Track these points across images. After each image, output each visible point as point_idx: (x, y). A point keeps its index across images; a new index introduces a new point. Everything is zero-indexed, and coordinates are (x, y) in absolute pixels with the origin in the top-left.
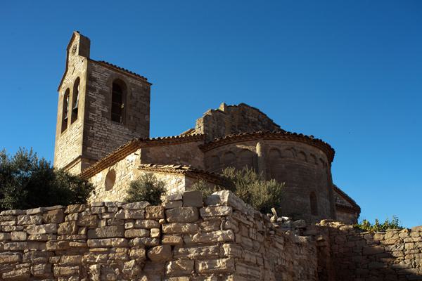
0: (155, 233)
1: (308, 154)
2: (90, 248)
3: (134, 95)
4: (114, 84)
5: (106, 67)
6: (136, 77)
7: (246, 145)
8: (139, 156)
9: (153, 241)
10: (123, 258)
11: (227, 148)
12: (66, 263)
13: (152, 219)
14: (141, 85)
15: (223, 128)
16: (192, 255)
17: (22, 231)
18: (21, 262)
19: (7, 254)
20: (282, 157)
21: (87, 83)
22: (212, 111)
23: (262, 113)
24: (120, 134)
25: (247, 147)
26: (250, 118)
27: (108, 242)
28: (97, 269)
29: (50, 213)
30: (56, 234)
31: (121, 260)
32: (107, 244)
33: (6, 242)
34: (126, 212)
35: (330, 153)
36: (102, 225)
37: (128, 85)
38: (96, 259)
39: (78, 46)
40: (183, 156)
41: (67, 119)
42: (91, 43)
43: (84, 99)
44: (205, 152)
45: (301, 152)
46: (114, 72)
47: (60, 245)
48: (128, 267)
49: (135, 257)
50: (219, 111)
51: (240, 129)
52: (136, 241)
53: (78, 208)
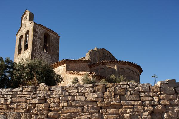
0: (156, 99)
1: (134, 71)
2: (123, 105)
3: (53, 41)
4: (44, 35)
5: (42, 27)
6: (54, 33)
7: (110, 65)
8: (66, 67)
9: (156, 103)
10: (142, 111)
11: (101, 66)
12: (110, 113)
13: (153, 92)
14: (56, 37)
15: (97, 58)
16: (176, 110)
17: (82, 95)
18: (83, 112)
19: (74, 108)
20: (125, 72)
21: (33, 33)
22: (93, 50)
23: (111, 53)
24: (46, 57)
25: (110, 67)
26: (106, 55)
27: (133, 103)
28: (129, 116)
29: (98, 87)
30: (103, 98)
31: (141, 112)
32: (132, 104)
33: (73, 101)
34: (140, 88)
35: (141, 70)
36: (128, 94)
38: (127, 111)
40: (82, 69)
41: (21, 49)
42: (34, 16)
43: (32, 40)
44: (90, 68)
45: (132, 71)
46: (45, 30)
47: (106, 104)
48: (145, 116)
49: (148, 110)
50: (95, 50)
51: (103, 59)
52: (147, 102)
53: (114, 85)
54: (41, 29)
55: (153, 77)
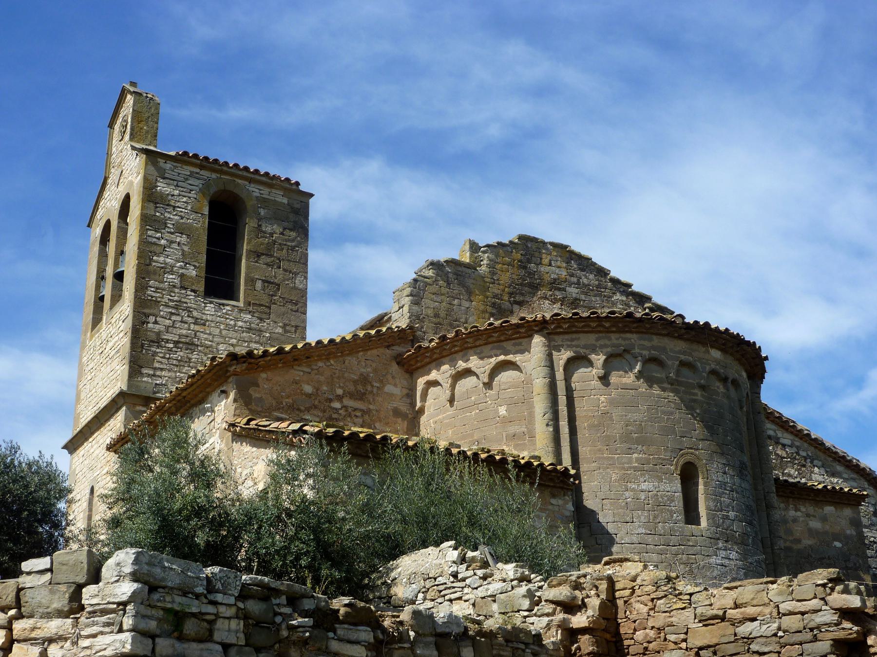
37: (250, 204)
39: (129, 120)
40: (351, 387)
46: (214, 176)
54: (192, 175)
55: (40, 452)
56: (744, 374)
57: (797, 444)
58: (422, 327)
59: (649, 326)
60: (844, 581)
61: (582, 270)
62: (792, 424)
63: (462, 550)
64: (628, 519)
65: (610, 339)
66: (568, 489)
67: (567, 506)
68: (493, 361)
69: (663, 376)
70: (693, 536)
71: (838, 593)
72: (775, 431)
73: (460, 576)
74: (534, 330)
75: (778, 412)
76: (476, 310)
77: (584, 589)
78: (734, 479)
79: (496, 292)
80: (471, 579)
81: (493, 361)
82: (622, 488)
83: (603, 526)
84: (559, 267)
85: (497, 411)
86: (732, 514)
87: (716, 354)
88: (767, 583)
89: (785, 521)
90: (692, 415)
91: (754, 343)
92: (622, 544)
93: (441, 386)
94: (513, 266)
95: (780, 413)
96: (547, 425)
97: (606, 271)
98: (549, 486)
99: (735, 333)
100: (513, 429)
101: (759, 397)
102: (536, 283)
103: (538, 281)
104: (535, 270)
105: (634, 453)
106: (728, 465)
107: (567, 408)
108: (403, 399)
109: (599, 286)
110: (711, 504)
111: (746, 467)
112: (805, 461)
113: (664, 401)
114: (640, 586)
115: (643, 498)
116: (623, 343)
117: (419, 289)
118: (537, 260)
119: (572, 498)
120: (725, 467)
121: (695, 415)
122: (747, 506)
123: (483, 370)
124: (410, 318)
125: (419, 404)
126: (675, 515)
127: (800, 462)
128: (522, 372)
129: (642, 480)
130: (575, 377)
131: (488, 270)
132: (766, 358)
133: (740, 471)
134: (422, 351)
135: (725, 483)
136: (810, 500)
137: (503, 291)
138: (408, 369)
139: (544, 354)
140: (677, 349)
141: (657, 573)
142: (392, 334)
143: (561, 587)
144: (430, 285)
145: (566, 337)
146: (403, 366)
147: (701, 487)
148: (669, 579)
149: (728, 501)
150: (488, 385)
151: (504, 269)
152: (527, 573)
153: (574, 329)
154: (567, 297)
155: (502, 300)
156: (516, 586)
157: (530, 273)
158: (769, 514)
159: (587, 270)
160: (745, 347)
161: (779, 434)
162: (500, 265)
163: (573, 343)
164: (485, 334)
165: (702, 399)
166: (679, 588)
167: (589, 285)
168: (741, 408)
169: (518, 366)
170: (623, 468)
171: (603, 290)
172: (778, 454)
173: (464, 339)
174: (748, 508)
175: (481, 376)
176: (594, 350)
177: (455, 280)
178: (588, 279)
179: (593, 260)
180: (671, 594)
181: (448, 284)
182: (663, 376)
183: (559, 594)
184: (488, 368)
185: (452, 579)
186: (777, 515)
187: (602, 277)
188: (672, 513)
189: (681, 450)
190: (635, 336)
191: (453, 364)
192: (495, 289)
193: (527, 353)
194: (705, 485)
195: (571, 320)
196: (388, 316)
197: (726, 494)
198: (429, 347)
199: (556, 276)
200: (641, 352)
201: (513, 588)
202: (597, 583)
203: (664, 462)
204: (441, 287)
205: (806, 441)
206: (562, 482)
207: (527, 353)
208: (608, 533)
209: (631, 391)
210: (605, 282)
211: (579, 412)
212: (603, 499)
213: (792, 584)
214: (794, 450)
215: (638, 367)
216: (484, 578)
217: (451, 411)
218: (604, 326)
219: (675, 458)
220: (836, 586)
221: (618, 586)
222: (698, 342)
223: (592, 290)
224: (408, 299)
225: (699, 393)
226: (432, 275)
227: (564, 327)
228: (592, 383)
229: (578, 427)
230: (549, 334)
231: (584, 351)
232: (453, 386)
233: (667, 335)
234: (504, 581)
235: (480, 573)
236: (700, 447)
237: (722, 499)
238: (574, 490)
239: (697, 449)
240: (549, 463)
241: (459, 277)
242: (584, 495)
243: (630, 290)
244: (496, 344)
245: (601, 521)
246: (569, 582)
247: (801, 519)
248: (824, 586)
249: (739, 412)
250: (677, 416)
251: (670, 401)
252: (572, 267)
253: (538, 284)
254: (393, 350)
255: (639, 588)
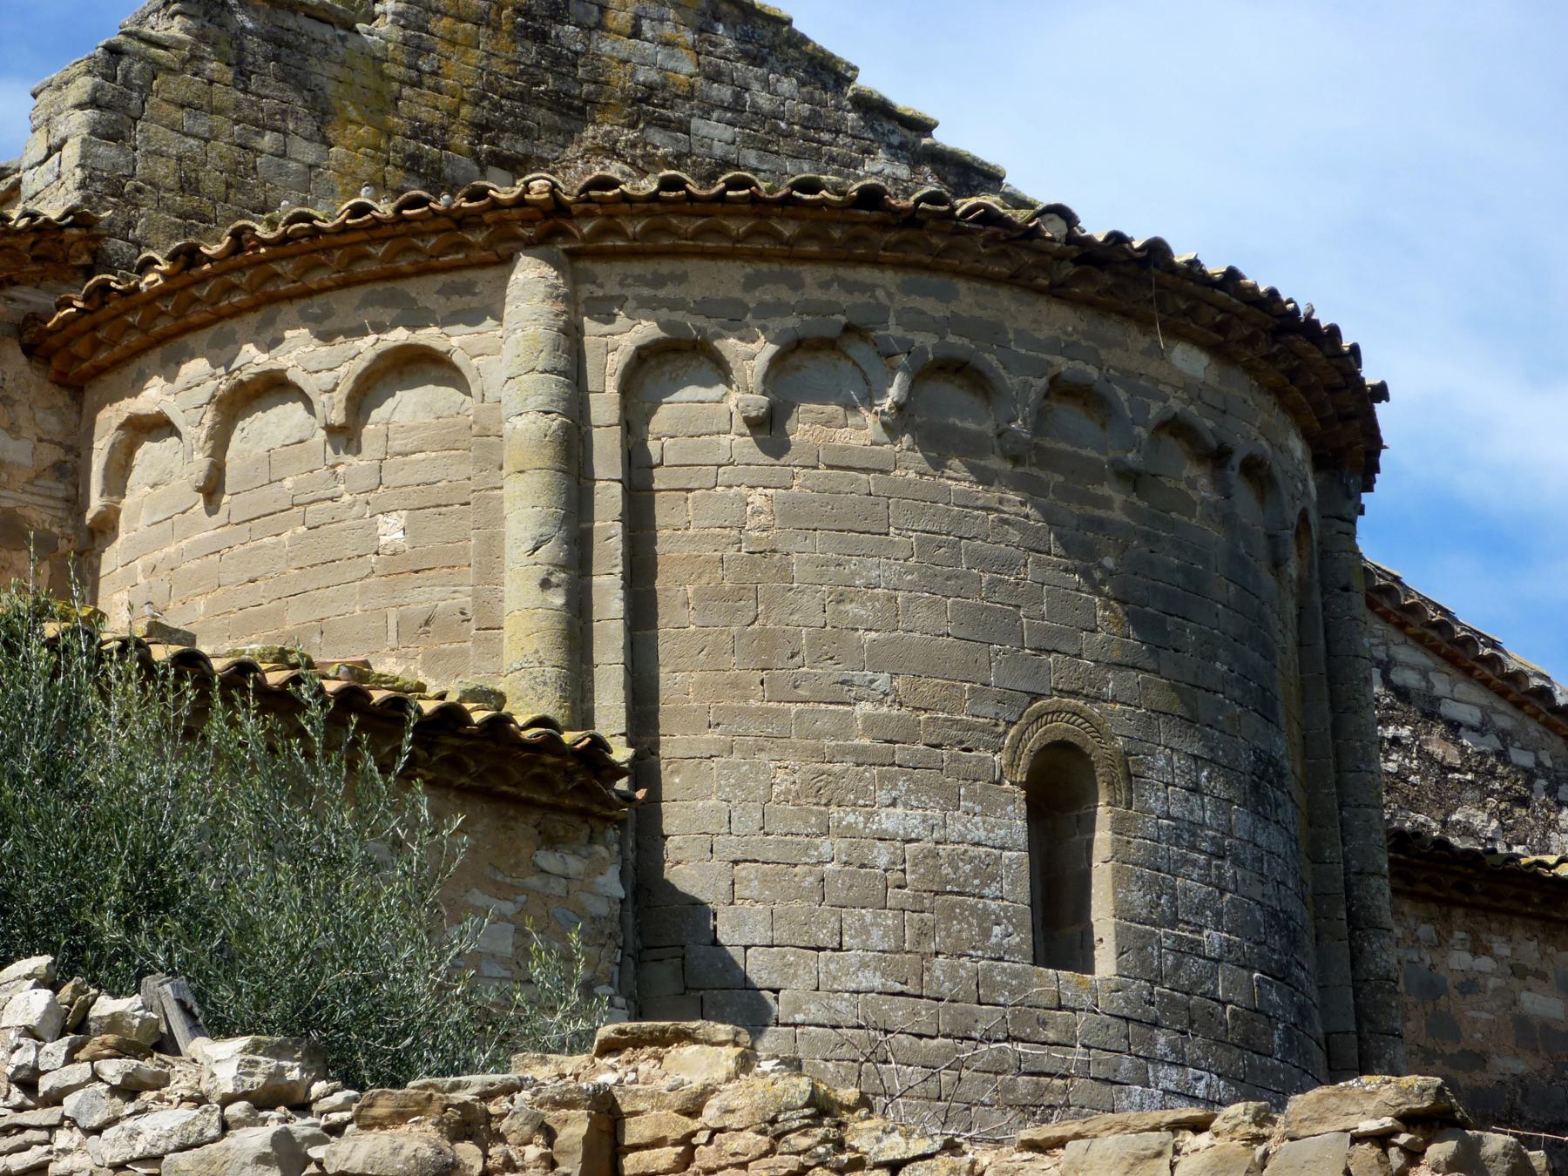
56: (1297, 446)
57: (1503, 722)
58: (130, 225)
59: (942, 245)
60: (1464, 1125)
61: (755, 60)
62: (1487, 651)
63: (77, 990)
64: (823, 937)
65: (796, 284)
66: (607, 819)
67: (600, 879)
68: (368, 347)
69: (988, 428)
70: (1060, 1008)
71: (1436, 1170)
72: (1424, 674)
73: (45, 1084)
74: (517, 238)
75: (1438, 607)
76: (343, 175)
77: (500, 1138)
78: (1227, 812)
79: (423, 116)
80: (79, 1094)
81: (368, 347)
82: (806, 822)
83: (731, 959)
84: (668, 44)
85: (371, 533)
86: (1212, 939)
87: (1190, 361)
88: (1176, 1127)
89: (1432, 988)
90: (1086, 575)
91: (1334, 331)
92: (796, 1025)
93: (178, 434)
94: (497, 29)
95: (1446, 612)
96: (545, 584)
97: (841, 68)
98: (529, 804)
99: (1262, 289)
100: (425, 597)
101: (1351, 535)
102: (578, 97)
103: (585, 88)
104: (579, 47)
105: (858, 699)
106: (1211, 761)
107: (624, 527)
108: (40, 482)
109: (810, 122)
110: (1136, 896)
111: (1281, 775)
112: (1529, 783)
113: (985, 520)
114: (714, 1132)
115: (883, 861)
116: (845, 299)
117: (127, 82)
118: (588, 13)
119: (621, 852)
120: (1199, 770)
121: (1098, 575)
122: (1274, 914)
123: (326, 378)
124: (82, 186)
125: (96, 502)
126: (997, 930)
127: (1508, 789)
128: (465, 388)
129: (883, 796)
130: (663, 418)
131: (397, 34)
132: (1381, 392)
133: (1255, 787)
134: (115, 304)
135: (1196, 827)
136: (1528, 915)
137: (453, 114)
138: (64, 374)
139: (549, 327)
140: (1044, 333)
141: (780, 1085)
142: (9, 240)
143: (405, 1128)
144: (170, 71)
145: (637, 268)
146: (47, 360)
147: (1103, 837)
148: (821, 1108)
149: (1199, 890)
150: (345, 436)
151: (460, 37)
152: (295, 1075)
153: (666, 241)
154: (689, 154)
155: (445, 147)
156: (241, 1123)
157: (557, 59)
158: (1361, 951)
159: (772, 59)
160: (1302, 344)
161: (1441, 685)
162: (446, 22)
163: (662, 293)
164: (340, 247)
165: (1126, 519)
166: (855, 1143)
167: (777, 116)
168: (1277, 564)
169: (456, 369)
170: (817, 753)
171: (826, 136)
172: (1430, 756)
173: (263, 262)
174: (1278, 920)
175: (320, 401)
176: (736, 323)
177: (267, 59)
178: (774, 93)
179: (795, 25)
180: (822, 1164)
181: (241, 73)
182: (988, 428)
183: (387, 1152)
184: (348, 372)
185: (17, 1096)
186: (1388, 955)
187: (825, 88)
188: (986, 921)
189: (1036, 697)
190: (889, 278)
191: (222, 357)
192: (422, 107)
193: (489, 322)
194: (1119, 826)
195: (657, 206)
196: (11, 180)
197: (1194, 863)
198: (136, 289)
199: (654, 76)
200: (910, 336)
201: (225, 1127)
202: (551, 1116)
203: (970, 738)
204: (211, 82)
205: (1535, 716)
206: (582, 789)
207: (489, 322)
208: (746, 985)
209: (864, 476)
210: (838, 108)
211: (667, 545)
212: (736, 862)
213: (1265, 1131)
214: (1491, 743)
215: (894, 392)
216: (128, 1090)
217: (207, 529)
218: (776, 236)
219: (1010, 724)
220: (1428, 1143)
221: (635, 1131)
222: (1127, 315)
223: (788, 135)
224: (81, 118)
225: (1118, 498)
226: (181, 35)
227: (630, 230)
228: (725, 440)
229: (660, 598)
230: (573, 255)
231: (701, 321)
232: (220, 439)
233: (1013, 280)
234: (199, 1100)
235: (113, 1070)
236: (1109, 690)
237: (1179, 882)
238: (631, 826)
239: (1096, 699)
240: (530, 717)
241: (284, 51)
242: (669, 845)
243: (925, 141)
244: (380, 287)
245: (723, 937)
246: (436, 1106)
247: (1492, 983)
248: (1382, 1139)
249: (1268, 579)
250: (1029, 574)
251: (1005, 522)
252: (715, 45)
253: (587, 101)
254: (13, 300)
255: (709, 1142)
